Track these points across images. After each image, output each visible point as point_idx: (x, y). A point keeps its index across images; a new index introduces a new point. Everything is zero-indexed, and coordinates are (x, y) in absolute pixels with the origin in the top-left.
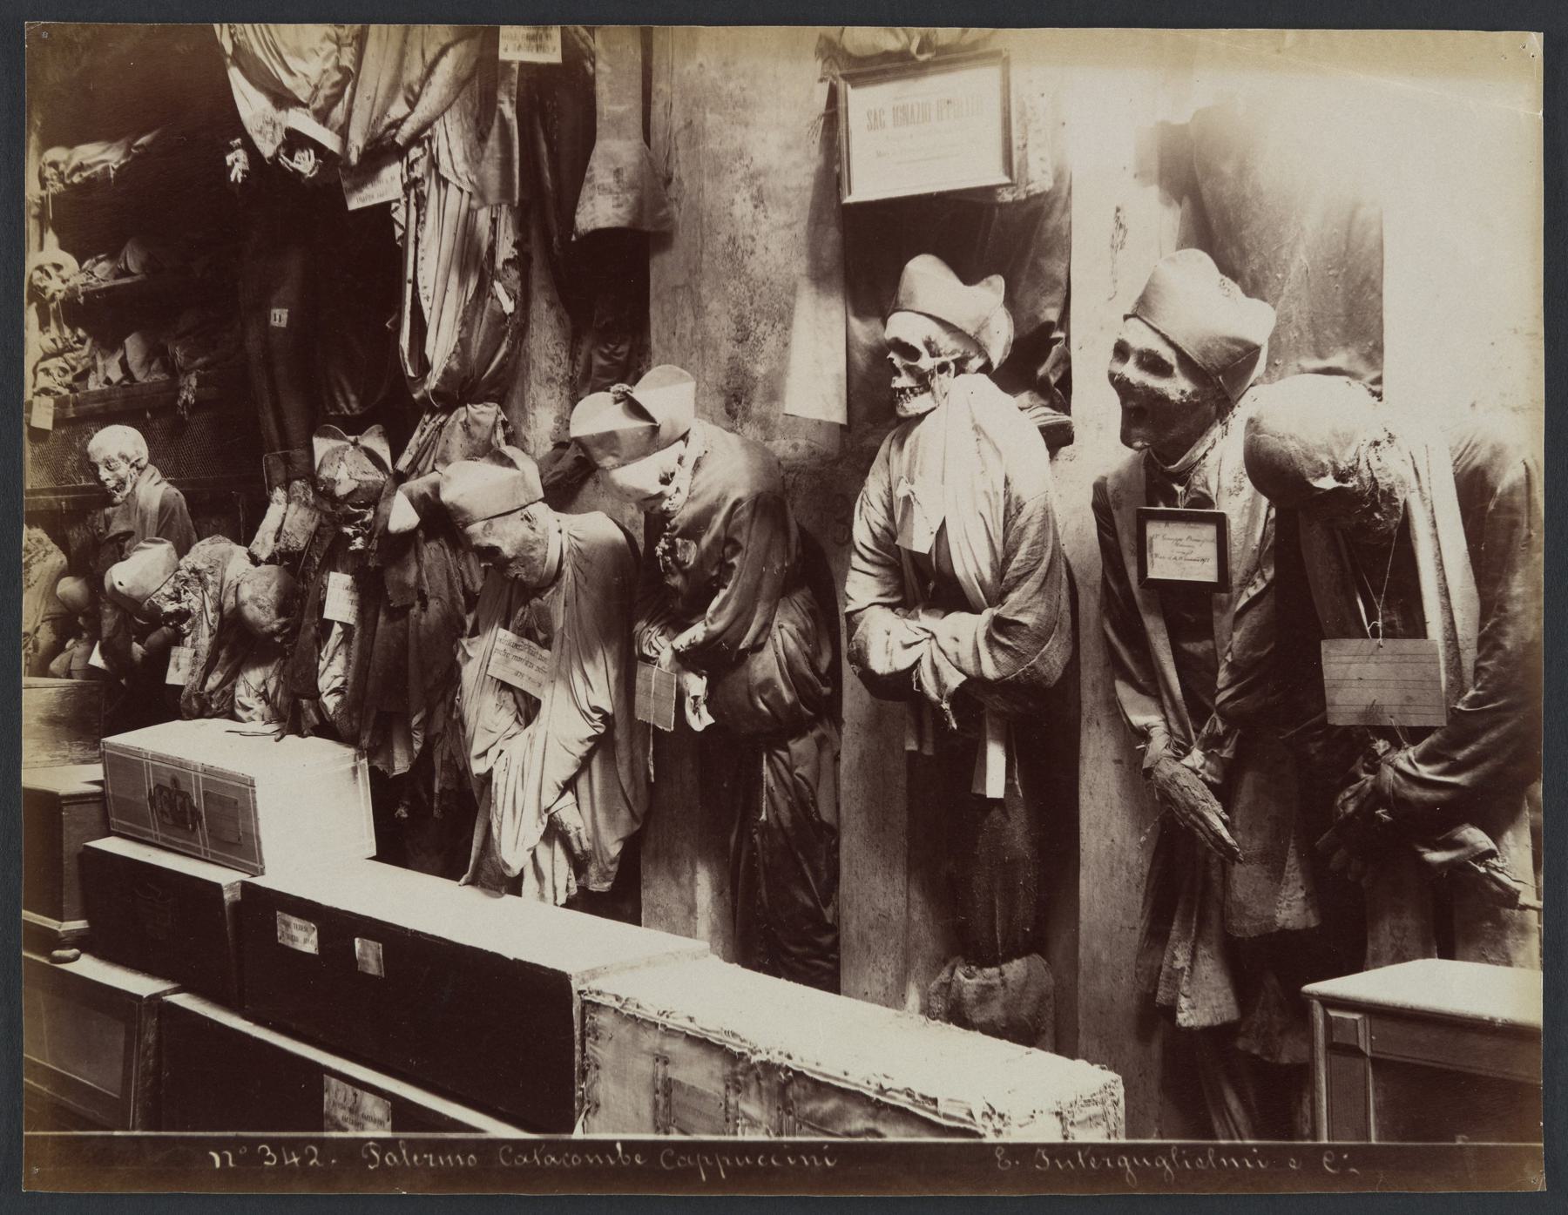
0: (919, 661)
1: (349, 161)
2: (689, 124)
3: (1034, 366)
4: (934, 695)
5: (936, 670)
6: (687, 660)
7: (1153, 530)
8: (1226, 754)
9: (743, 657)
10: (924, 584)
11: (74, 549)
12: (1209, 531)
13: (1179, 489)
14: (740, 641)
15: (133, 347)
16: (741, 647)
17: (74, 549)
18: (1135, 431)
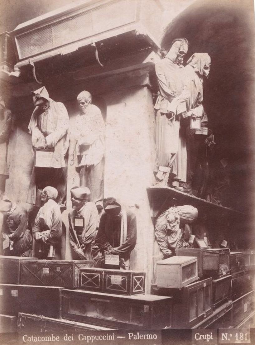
0: (42, 238)
2: (13, 160)
3: (61, 198)
4: (44, 241)
5: (44, 238)
6: (11, 239)
7: (76, 220)
8: (84, 249)
9: (20, 239)
10: (43, 227)
12: (82, 220)
13: (79, 214)
18: (74, 206)
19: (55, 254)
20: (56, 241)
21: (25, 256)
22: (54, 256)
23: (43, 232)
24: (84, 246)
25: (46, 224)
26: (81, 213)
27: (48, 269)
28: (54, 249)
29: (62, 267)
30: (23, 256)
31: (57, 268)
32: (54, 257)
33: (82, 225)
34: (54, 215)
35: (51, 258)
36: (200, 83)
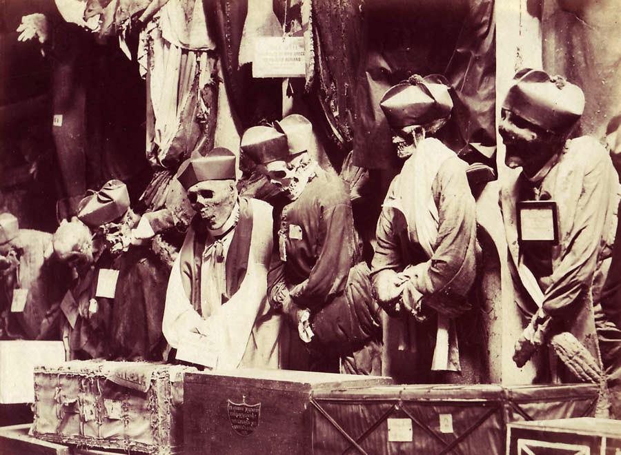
0: (402, 293)
7: (524, 213)
10: (407, 252)
11: (7, 311)
12: (549, 212)
15: (151, 160)
16: (330, 292)
17: (7, 311)
19: (456, 357)
20: (461, 305)
22: (455, 364)
23: (407, 271)
24: (545, 319)
27: (407, 423)
28: (451, 342)
29: (462, 415)
30: (348, 371)
31: (442, 417)
32: (453, 368)
33: (549, 236)
34: (442, 197)
35: (443, 377)
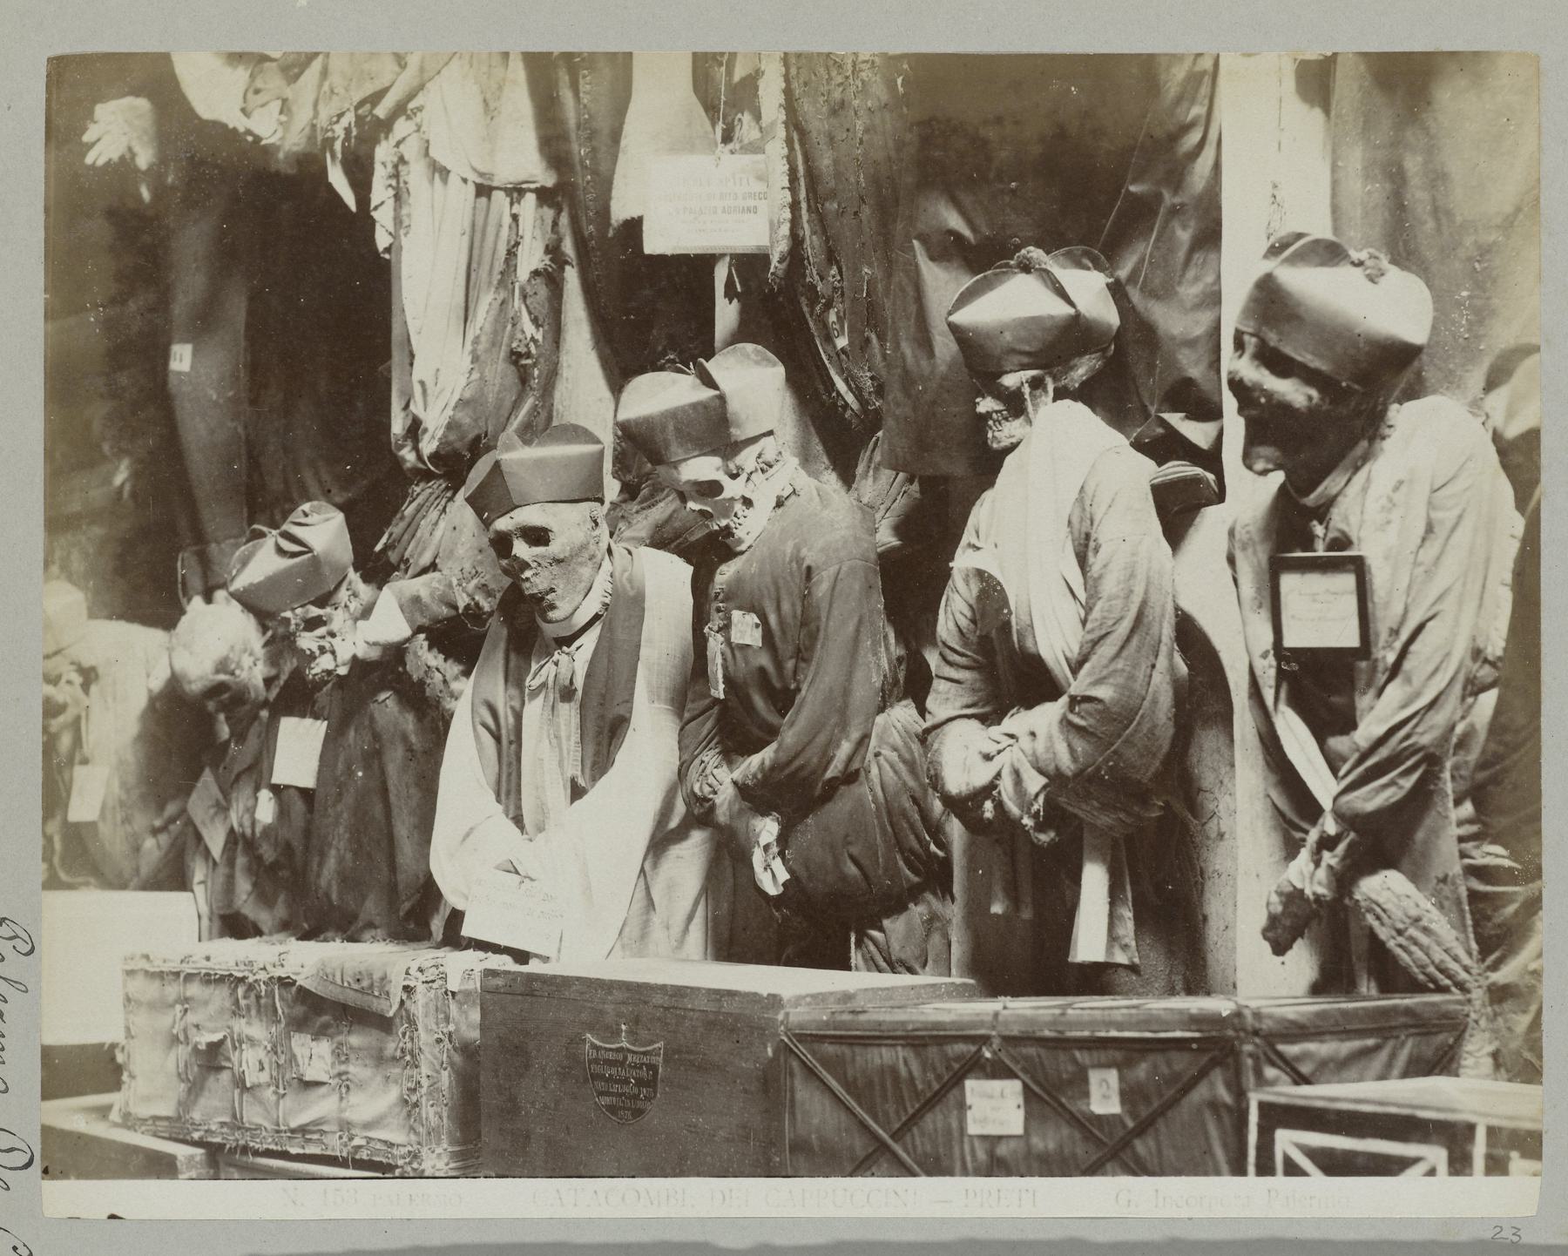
0: (998, 775)
1: (84, 155)
5: (1017, 773)
7: (1290, 583)
12: (1348, 581)
14: (826, 769)
16: (829, 774)
19: (1127, 929)
21: (894, 965)
22: (1125, 947)
25: (1029, 644)
26: (1336, 514)
29: (1142, 1071)
31: (1095, 1077)
32: (1121, 958)
36: (450, 662)
